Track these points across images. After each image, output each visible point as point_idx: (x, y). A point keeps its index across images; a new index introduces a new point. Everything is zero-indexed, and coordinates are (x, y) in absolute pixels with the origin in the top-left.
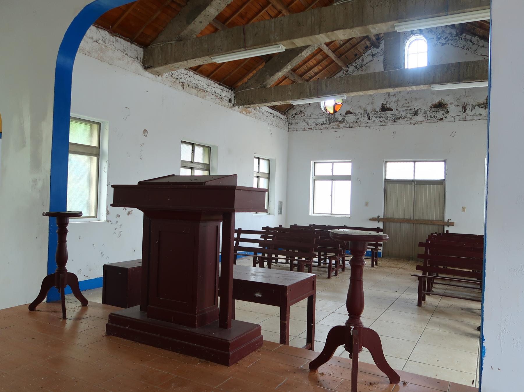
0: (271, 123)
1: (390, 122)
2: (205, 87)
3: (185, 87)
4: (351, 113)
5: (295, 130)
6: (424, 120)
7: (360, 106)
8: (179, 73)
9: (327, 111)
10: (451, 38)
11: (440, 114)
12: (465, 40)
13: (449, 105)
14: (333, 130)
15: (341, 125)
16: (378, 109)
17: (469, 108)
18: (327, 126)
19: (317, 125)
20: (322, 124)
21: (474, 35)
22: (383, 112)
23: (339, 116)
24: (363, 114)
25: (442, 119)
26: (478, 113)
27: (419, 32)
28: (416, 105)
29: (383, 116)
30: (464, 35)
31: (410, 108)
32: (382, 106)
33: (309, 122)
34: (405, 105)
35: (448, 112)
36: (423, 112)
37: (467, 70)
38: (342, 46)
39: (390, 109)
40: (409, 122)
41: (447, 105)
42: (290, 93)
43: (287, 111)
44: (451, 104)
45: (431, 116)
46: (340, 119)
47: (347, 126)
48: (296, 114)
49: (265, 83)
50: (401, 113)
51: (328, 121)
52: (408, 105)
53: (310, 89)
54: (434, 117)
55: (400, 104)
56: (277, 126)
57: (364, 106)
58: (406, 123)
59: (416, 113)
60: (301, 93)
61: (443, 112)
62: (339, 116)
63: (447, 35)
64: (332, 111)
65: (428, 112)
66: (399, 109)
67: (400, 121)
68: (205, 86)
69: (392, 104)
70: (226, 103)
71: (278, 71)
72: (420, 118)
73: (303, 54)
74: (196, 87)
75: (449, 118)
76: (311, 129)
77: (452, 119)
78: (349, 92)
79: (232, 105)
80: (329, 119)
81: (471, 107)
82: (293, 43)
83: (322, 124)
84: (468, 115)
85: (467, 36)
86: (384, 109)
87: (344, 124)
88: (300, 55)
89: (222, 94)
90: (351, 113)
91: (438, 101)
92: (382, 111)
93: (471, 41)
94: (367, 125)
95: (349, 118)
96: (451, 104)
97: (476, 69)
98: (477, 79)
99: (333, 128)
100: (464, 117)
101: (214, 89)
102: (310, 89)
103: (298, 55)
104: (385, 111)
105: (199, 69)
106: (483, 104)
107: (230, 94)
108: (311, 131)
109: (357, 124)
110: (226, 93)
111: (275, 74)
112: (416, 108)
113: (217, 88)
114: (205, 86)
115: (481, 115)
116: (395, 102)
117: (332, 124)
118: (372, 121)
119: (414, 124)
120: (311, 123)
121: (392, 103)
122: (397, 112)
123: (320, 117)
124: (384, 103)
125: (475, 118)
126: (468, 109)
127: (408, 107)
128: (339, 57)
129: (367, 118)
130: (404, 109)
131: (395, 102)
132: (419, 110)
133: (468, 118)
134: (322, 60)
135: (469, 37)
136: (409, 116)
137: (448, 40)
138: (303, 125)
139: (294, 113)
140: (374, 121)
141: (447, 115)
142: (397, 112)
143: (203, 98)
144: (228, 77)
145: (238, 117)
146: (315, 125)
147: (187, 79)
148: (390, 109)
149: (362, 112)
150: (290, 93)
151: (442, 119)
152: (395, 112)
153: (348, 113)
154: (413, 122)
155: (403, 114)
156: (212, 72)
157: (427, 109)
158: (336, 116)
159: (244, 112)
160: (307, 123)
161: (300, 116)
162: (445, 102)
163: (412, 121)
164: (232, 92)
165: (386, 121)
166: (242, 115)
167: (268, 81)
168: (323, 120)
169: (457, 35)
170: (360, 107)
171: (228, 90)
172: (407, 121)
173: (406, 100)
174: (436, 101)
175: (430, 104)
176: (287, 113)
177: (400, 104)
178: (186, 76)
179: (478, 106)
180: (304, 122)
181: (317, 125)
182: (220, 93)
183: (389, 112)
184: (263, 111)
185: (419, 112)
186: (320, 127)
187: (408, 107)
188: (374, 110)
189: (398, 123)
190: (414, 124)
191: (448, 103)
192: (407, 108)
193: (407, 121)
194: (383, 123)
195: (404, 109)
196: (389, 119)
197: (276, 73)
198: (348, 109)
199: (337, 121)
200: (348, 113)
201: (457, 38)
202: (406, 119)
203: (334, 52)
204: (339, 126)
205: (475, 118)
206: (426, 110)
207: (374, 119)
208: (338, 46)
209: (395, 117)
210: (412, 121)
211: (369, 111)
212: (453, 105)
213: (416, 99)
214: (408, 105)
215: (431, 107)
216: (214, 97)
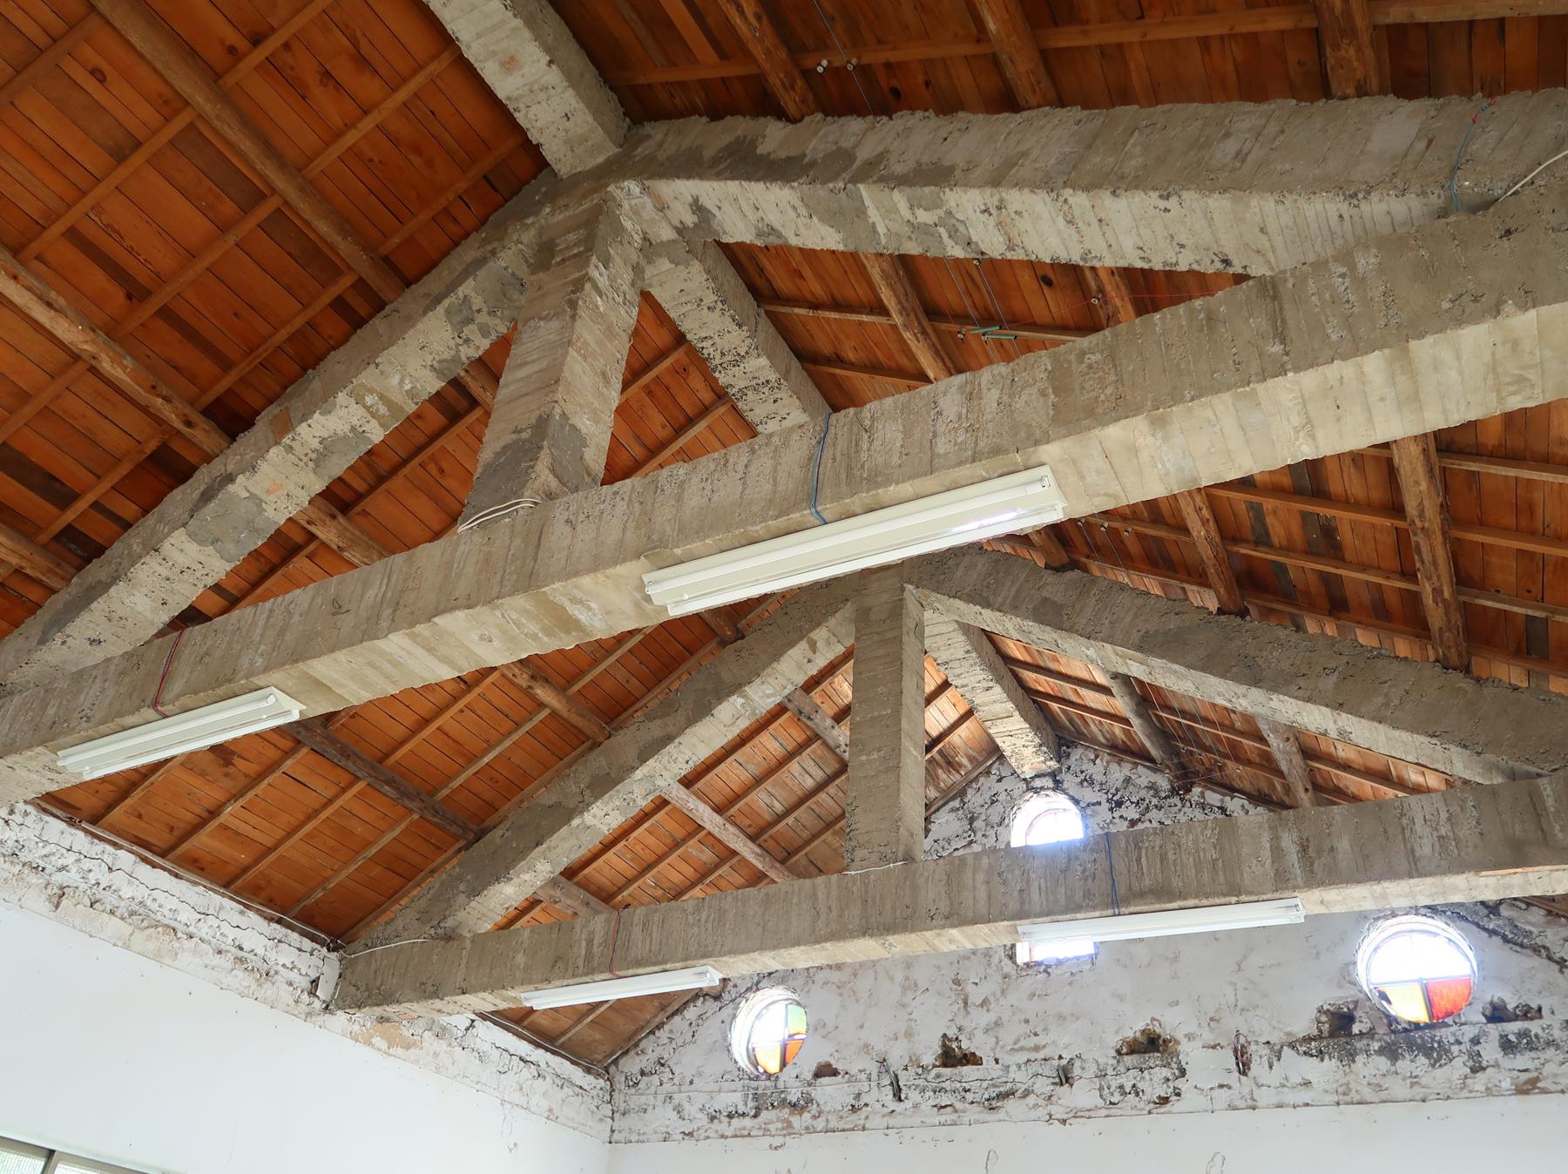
0: (517, 1098)
1: (974, 1113)
2: (183, 917)
3: (64, 902)
4: (835, 1073)
5: (634, 1138)
6: (1100, 1103)
7: (866, 1046)
8: (52, 848)
9: (756, 1064)
10: (1155, 801)
11: (1155, 1080)
12: (1203, 806)
13: (1184, 1041)
14: (768, 1140)
15: (797, 1121)
16: (928, 1059)
17: (1259, 1055)
18: (747, 1122)
19: (712, 1118)
20: (730, 1116)
21: (1230, 789)
22: (947, 1071)
23: (792, 1082)
24: (874, 1077)
25: (1164, 1101)
26: (1296, 1079)
27: (1049, 782)
28: (1063, 1043)
29: (947, 1085)
30: (1196, 790)
31: (1041, 1055)
32: (944, 1045)
33: (686, 1105)
34: (1022, 1043)
35: (1183, 1073)
36: (1092, 1069)
37: (1139, 860)
38: (780, 818)
39: (970, 1059)
40: (1042, 1113)
41: (1177, 1042)
42: (520, 959)
43: (615, 1062)
44: (1190, 1037)
45: (1121, 1087)
46: (793, 1099)
47: (820, 1124)
48: (643, 1073)
49: (449, 923)
50: (1014, 1074)
51: (751, 1104)
52: (1034, 1041)
53: (590, 942)
54: (1136, 1091)
55: (1007, 1037)
56: (551, 1116)
57: (879, 1045)
58: (1034, 1114)
59: (1065, 1077)
60: (558, 959)
61: (1166, 1072)
62: (792, 1082)
63: (1143, 793)
64: (774, 1067)
65: (1110, 1071)
66: (1006, 1059)
67: (1011, 1105)
68: (186, 915)
69: (980, 1037)
70: (286, 994)
71: (498, 880)
72: (1082, 1094)
73: (588, 818)
74: (138, 915)
75: (1190, 1099)
76: (690, 1134)
77: (1203, 1102)
78: (720, 955)
79: (318, 1005)
80: (756, 1097)
81: (1265, 1051)
82: (319, 685)
83: (730, 1116)
84: (1259, 1086)
85: (1208, 793)
86: (952, 1057)
87: (806, 1116)
88: (576, 822)
89: (272, 955)
90: (835, 1073)
91: (1141, 1026)
92: (945, 1065)
93: (1223, 810)
94: (891, 1121)
95: (830, 1093)
96: (1190, 1037)
97: (1171, 857)
98: (1182, 896)
99: (766, 1132)
100: (1246, 1091)
101: (232, 933)
102: (590, 942)
103: (569, 820)
104: (953, 1066)
105: (179, 851)
106: (1308, 1039)
107: (315, 960)
108: (689, 1142)
109: (854, 1117)
110: (295, 956)
111: (485, 888)
112: (1067, 1056)
113: (252, 930)
114: (186, 915)
115: (1307, 1084)
116: (987, 1031)
117: (764, 1115)
118: (908, 1104)
119: (1064, 1122)
120: (691, 1110)
121: (979, 1035)
122: (996, 1071)
123: (725, 1085)
124: (951, 1034)
125: (1290, 1097)
126: (1255, 1058)
127: (1036, 1049)
128: (783, 862)
129: (889, 1091)
130: (1022, 1058)
131: (987, 1031)
132: (1077, 1063)
133: (1265, 1097)
134: (717, 867)
135: (1213, 798)
136: (1043, 1086)
137: (1147, 809)
138: (663, 1117)
139: (636, 1070)
140: (915, 1106)
141: (1180, 1083)
142: (996, 1071)
143: (157, 957)
144: (319, 894)
145: (341, 1050)
146: (705, 1120)
147: (92, 878)
148: (970, 1059)
149: (873, 1068)
150: (520, 959)
151: (1164, 1101)
152: (988, 1069)
153: (825, 1071)
154: (1058, 1112)
155: (1021, 1077)
156: (245, 870)
157: (1107, 1058)
158: (781, 1085)
159: (377, 1041)
160: (679, 1110)
161: (655, 1079)
162: (1166, 1033)
163: (1054, 1109)
164: (334, 956)
165: (958, 1105)
166: (361, 1049)
167: (461, 915)
168: (732, 1099)
169: (1174, 792)
170: (867, 1047)
171: (307, 944)
172: (1036, 1106)
173: (1027, 1021)
174: (1134, 1028)
175: (1114, 1041)
176: (612, 1069)
177: (1007, 1037)
178: (87, 864)
179: (1292, 1046)
180: (669, 1107)
181: (712, 1118)
182: (261, 951)
183: (966, 1070)
184: (486, 1047)
185: (1076, 1071)
186: (722, 1126)
187: (1036, 1049)
188: (915, 1061)
189: (1001, 1114)
190: (1064, 1122)
191: (1179, 1035)
192: (1033, 1056)
193: (1036, 1106)
194: (947, 1116)
195: (1022, 1058)
196: (969, 1096)
197: (490, 883)
198: (824, 1058)
199: (784, 1103)
200: (825, 1071)
201: (1176, 800)
202: (1031, 1099)
203: (753, 838)
204: (789, 1125)
205: (1290, 1097)
206: (1102, 1061)
207: (914, 1096)
208: (768, 817)
209: (993, 1092)
210: (1054, 1109)
211: (895, 1063)
212: (1198, 1044)
213: (1061, 1018)
214: (1034, 1041)
215: (1119, 1052)
216: (225, 962)
